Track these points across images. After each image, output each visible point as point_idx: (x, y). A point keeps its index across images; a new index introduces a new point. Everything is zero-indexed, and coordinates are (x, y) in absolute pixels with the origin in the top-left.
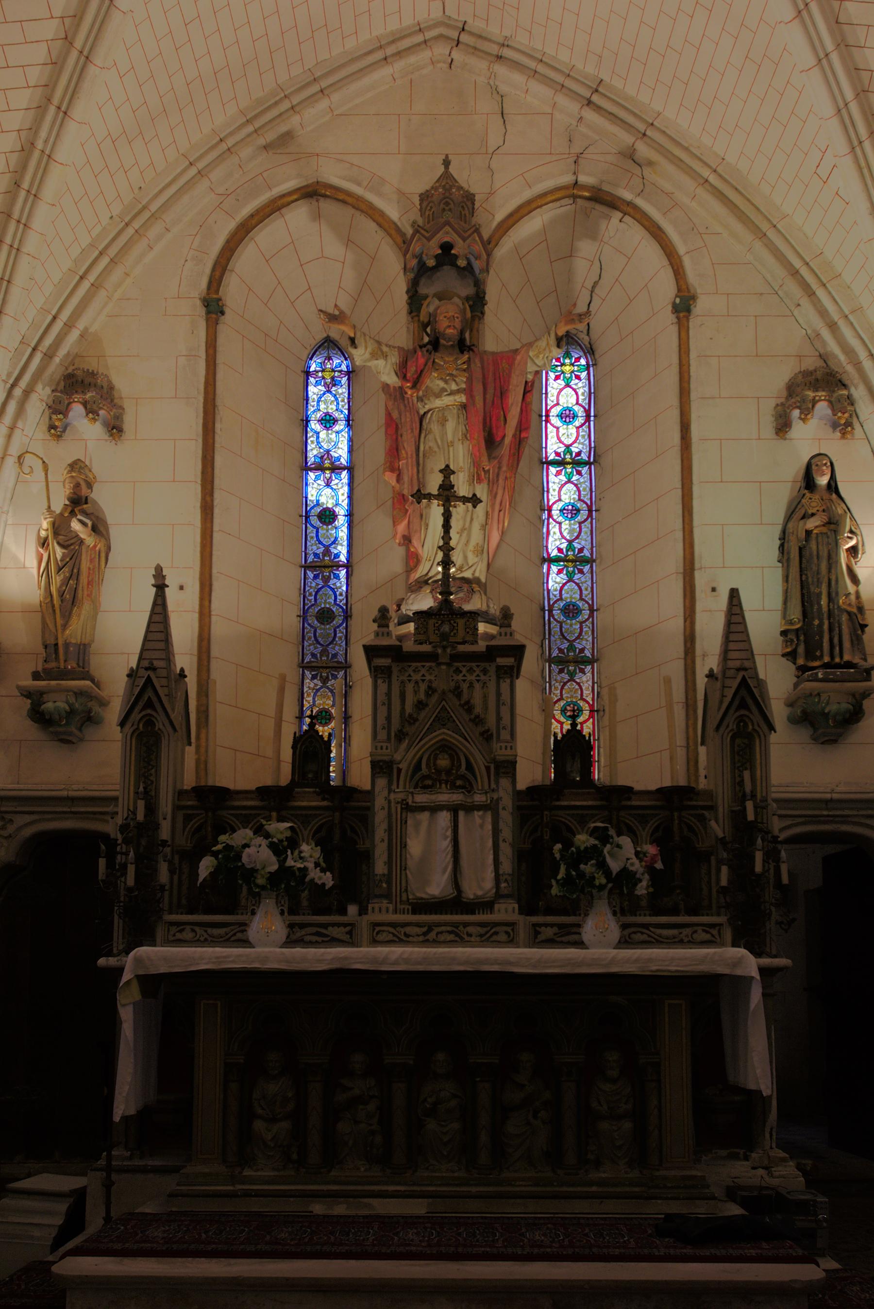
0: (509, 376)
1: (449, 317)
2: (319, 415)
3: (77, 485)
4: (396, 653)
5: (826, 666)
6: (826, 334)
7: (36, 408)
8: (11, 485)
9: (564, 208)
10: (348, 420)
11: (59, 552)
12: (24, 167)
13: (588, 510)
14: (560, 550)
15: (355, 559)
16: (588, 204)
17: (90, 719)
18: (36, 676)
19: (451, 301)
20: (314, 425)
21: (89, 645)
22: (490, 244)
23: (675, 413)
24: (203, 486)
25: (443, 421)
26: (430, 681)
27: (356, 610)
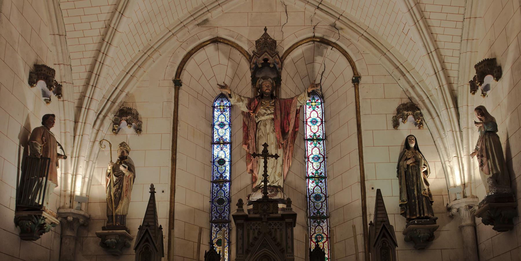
0: (290, 108)
1: (267, 86)
2: (218, 123)
3: (123, 152)
4: (246, 218)
5: (418, 218)
6: (410, 90)
7: (108, 122)
8: (97, 152)
9: (310, 45)
10: (229, 125)
11: (115, 178)
12: (106, 34)
13: (324, 158)
14: (313, 174)
15: (233, 178)
16: (319, 44)
17: (126, 246)
18: (104, 228)
19: (268, 79)
20: (216, 127)
21: (126, 215)
22: (282, 59)
23: (355, 120)
24: (172, 151)
25: (265, 125)
26: (259, 229)
27: (233, 198)
